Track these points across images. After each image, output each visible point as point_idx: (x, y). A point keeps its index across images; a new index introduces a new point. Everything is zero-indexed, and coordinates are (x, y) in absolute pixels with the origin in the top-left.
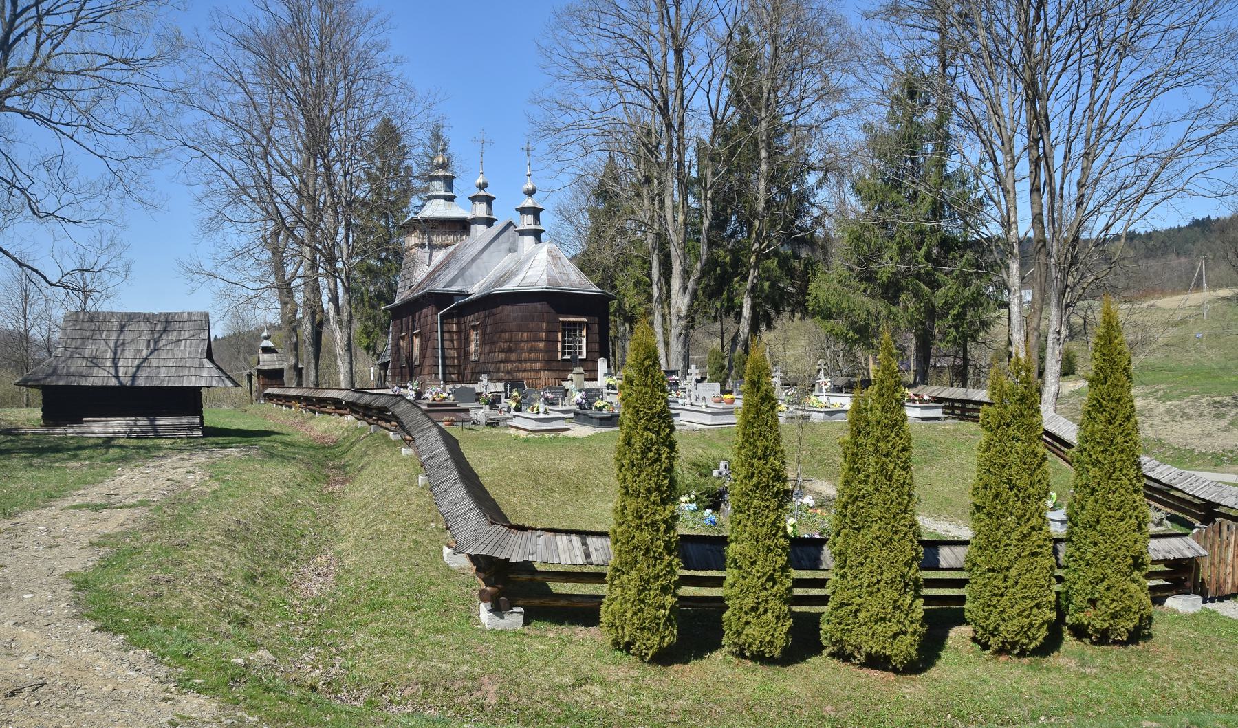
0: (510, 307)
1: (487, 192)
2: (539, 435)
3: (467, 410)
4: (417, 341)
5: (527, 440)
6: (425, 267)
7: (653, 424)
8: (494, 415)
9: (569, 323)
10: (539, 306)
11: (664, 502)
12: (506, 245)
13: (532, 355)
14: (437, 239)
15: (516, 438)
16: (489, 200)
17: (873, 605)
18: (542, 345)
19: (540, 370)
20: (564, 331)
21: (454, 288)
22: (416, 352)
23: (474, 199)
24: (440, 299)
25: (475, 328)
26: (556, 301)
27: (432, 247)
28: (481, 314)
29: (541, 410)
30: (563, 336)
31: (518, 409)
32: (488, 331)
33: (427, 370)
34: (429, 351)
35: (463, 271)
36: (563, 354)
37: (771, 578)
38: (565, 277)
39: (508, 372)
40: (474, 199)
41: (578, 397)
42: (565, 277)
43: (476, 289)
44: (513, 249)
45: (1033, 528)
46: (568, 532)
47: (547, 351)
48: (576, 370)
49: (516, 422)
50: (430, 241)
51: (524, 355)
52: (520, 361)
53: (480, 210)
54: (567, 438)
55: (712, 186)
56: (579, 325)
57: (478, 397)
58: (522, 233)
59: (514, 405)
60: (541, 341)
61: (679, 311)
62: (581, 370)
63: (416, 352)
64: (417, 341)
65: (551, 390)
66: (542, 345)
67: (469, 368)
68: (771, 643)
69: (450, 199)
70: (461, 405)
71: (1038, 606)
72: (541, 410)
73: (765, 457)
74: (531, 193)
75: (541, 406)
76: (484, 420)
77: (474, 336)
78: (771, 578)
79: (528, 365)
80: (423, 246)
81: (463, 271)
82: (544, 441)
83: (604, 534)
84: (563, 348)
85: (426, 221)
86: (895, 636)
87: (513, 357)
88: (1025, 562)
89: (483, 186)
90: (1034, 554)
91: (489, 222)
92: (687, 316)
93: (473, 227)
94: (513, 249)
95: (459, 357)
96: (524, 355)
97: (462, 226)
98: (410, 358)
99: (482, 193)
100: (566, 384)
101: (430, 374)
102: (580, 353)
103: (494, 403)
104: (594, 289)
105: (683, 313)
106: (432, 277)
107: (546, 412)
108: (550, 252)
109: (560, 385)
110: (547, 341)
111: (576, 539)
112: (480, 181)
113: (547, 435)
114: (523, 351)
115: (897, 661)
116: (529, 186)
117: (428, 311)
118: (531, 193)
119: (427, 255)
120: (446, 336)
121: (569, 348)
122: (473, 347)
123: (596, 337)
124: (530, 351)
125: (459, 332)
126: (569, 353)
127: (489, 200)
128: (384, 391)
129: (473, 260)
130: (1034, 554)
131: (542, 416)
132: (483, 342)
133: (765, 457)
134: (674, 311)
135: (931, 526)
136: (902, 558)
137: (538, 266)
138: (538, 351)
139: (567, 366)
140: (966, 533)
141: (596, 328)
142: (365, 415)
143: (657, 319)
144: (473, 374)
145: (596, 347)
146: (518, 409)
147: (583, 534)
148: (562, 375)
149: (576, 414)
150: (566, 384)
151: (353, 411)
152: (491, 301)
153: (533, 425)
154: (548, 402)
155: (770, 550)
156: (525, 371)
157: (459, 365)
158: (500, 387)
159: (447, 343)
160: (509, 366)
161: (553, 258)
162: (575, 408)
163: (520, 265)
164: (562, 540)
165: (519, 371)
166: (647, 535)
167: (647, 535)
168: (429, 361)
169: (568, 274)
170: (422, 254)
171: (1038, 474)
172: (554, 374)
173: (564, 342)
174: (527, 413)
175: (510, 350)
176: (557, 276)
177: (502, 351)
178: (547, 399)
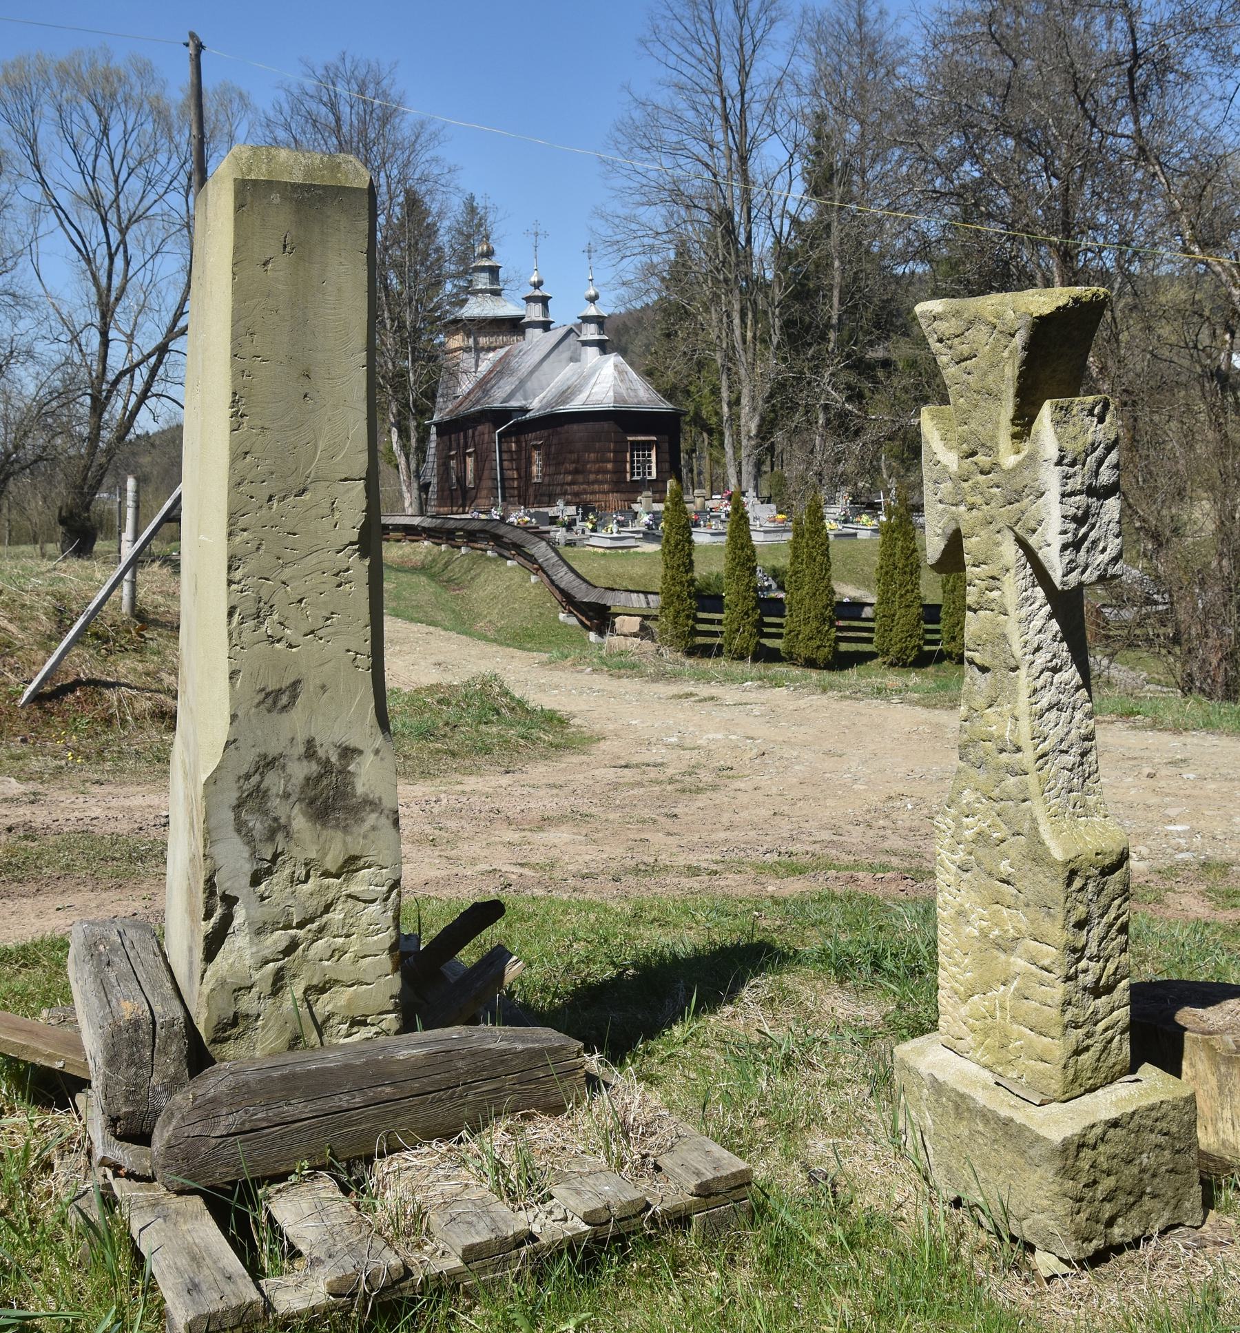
0: (575, 427)
1: (543, 291)
2: (613, 551)
3: (548, 532)
4: (470, 462)
5: (604, 554)
6: (470, 373)
7: (680, 531)
8: (571, 536)
9: (638, 442)
10: (606, 425)
11: (687, 572)
12: (567, 355)
13: (600, 477)
14: (483, 341)
15: (595, 553)
16: (544, 300)
17: (806, 631)
18: (609, 466)
19: (608, 493)
20: (632, 451)
21: (514, 404)
22: (470, 475)
23: (529, 299)
24: (499, 416)
25: (537, 447)
26: (623, 420)
27: (479, 350)
28: (545, 433)
29: (615, 530)
30: (632, 456)
31: (594, 530)
32: (553, 449)
33: (484, 493)
34: (486, 473)
35: (522, 382)
36: (632, 474)
37: (746, 613)
38: (632, 394)
39: (576, 494)
40: (529, 299)
41: (646, 518)
42: (632, 394)
43: (536, 405)
44: (575, 359)
45: (907, 591)
46: (638, 592)
47: (614, 472)
48: (645, 493)
49: (592, 541)
50: (476, 342)
51: (592, 477)
52: (588, 483)
53: (534, 313)
54: (637, 553)
55: (780, 303)
56: (647, 446)
57: (553, 520)
58: (585, 343)
59: (590, 526)
60: (609, 461)
61: (749, 431)
62: (650, 494)
63: (470, 475)
64: (470, 462)
65: (622, 513)
66: (609, 466)
67: (531, 491)
68: (747, 648)
69: (496, 293)
70: (543, 528)
71: (911, 636)
72: (615, 530)
73: (742, 549)
74: (593, 299)
75: (614, 527)
76: (562, 541)
77: (536, 457)
78: (746, 613)
79: (596, 487)
80: (467, 350)
81: (522, 382)
82: (617, 555)
83: (657, 593)
84: (632, 468)
85: (472, 320)
86: (818, 647)
87: (580, 478)
88: (903, 611)
89: (537, 285)
90: (909, 606)
91: (546, 326)
92: (757, 436)
93: (529, 331)
94: (575, 359)
95: (520, 477)
96: (592, 477)
97: (515, 326)
98: (462, 479)
99: (537, 293)
100: (636, 507)
101: (487, 497)
102: (650, 474)
103: (569, 526)
104: (665, 406)
105: (753, 433)
106: (484, 385)
107: (619, 532)
108: (616, 366)
109: (630, 508)
110: (615, 461)
111: (641, 596)
112: (534, 279)
113: (619, 551)
114: (591, 472)
115: (820, 662)
116: (592, 292)
117: (484, 428)
118: (593, 299)
119: (473, 361)
120: (505, 456)
121: (638, 468)
122: (534, 469)
123: (667, 456)
124: (598, 472)
125: (519, 451)
126: (638, 474)
127: (544, 300)
128: (463, 516)
129: (532, 372)
130: (909, 606)
131: (615, 535)
132: (546, 464)
133: (742, 549)
134: (744, 430)
135: (847, 592)
136: (821, 604)
137: (604, 382)
138: (605, 472)
139: (636, 488)
140: (873, 600)
141: (666, 446)
142: (448, 539)
143: (728, 440)
144: (536, 497)
145: (666, 466)
146: (594, 530)
147: (646, 593)
148: (631, 496)
149: (644, 533)
150: (636, 507)
151: (429, 537)
152: (554, 421)
153: (608, 543)
154: (621, 524)
155: (745, 598)
156: (593, 493)
157: (519, 488)
158: (572, 510)
159: (506, 463)
160: (576, 488)
161: (619, 373)
162: (643, 529)
163: (584, 379)
164: (634, 596)
165: (586, 493)
166: (678, 588)
167: (678, 588)
168: (487, 483)
169: (635, 390)
170: (467, 360)
171: (911, 560)
172: (624, 496)
173: (632, 462)
174: (603, 533)
175: (576, 472)
176: (624, 392)
177: (570, 473)
178: (618, 522)
